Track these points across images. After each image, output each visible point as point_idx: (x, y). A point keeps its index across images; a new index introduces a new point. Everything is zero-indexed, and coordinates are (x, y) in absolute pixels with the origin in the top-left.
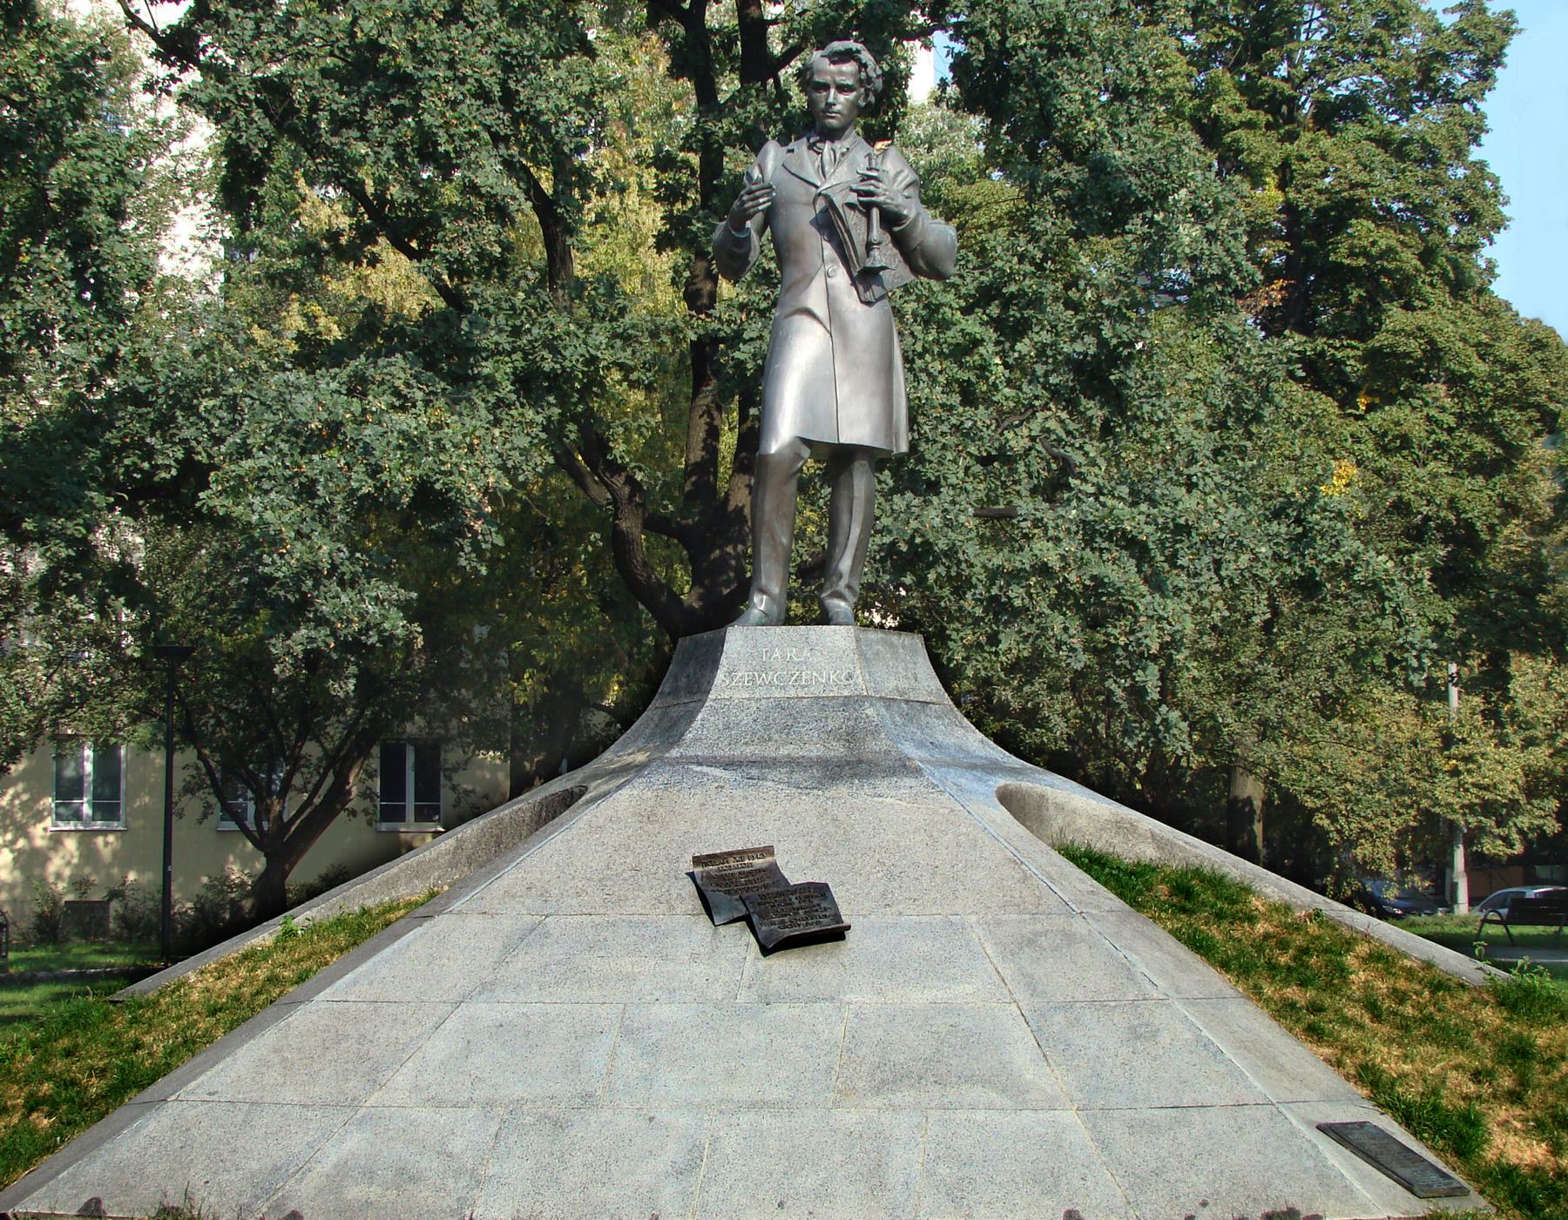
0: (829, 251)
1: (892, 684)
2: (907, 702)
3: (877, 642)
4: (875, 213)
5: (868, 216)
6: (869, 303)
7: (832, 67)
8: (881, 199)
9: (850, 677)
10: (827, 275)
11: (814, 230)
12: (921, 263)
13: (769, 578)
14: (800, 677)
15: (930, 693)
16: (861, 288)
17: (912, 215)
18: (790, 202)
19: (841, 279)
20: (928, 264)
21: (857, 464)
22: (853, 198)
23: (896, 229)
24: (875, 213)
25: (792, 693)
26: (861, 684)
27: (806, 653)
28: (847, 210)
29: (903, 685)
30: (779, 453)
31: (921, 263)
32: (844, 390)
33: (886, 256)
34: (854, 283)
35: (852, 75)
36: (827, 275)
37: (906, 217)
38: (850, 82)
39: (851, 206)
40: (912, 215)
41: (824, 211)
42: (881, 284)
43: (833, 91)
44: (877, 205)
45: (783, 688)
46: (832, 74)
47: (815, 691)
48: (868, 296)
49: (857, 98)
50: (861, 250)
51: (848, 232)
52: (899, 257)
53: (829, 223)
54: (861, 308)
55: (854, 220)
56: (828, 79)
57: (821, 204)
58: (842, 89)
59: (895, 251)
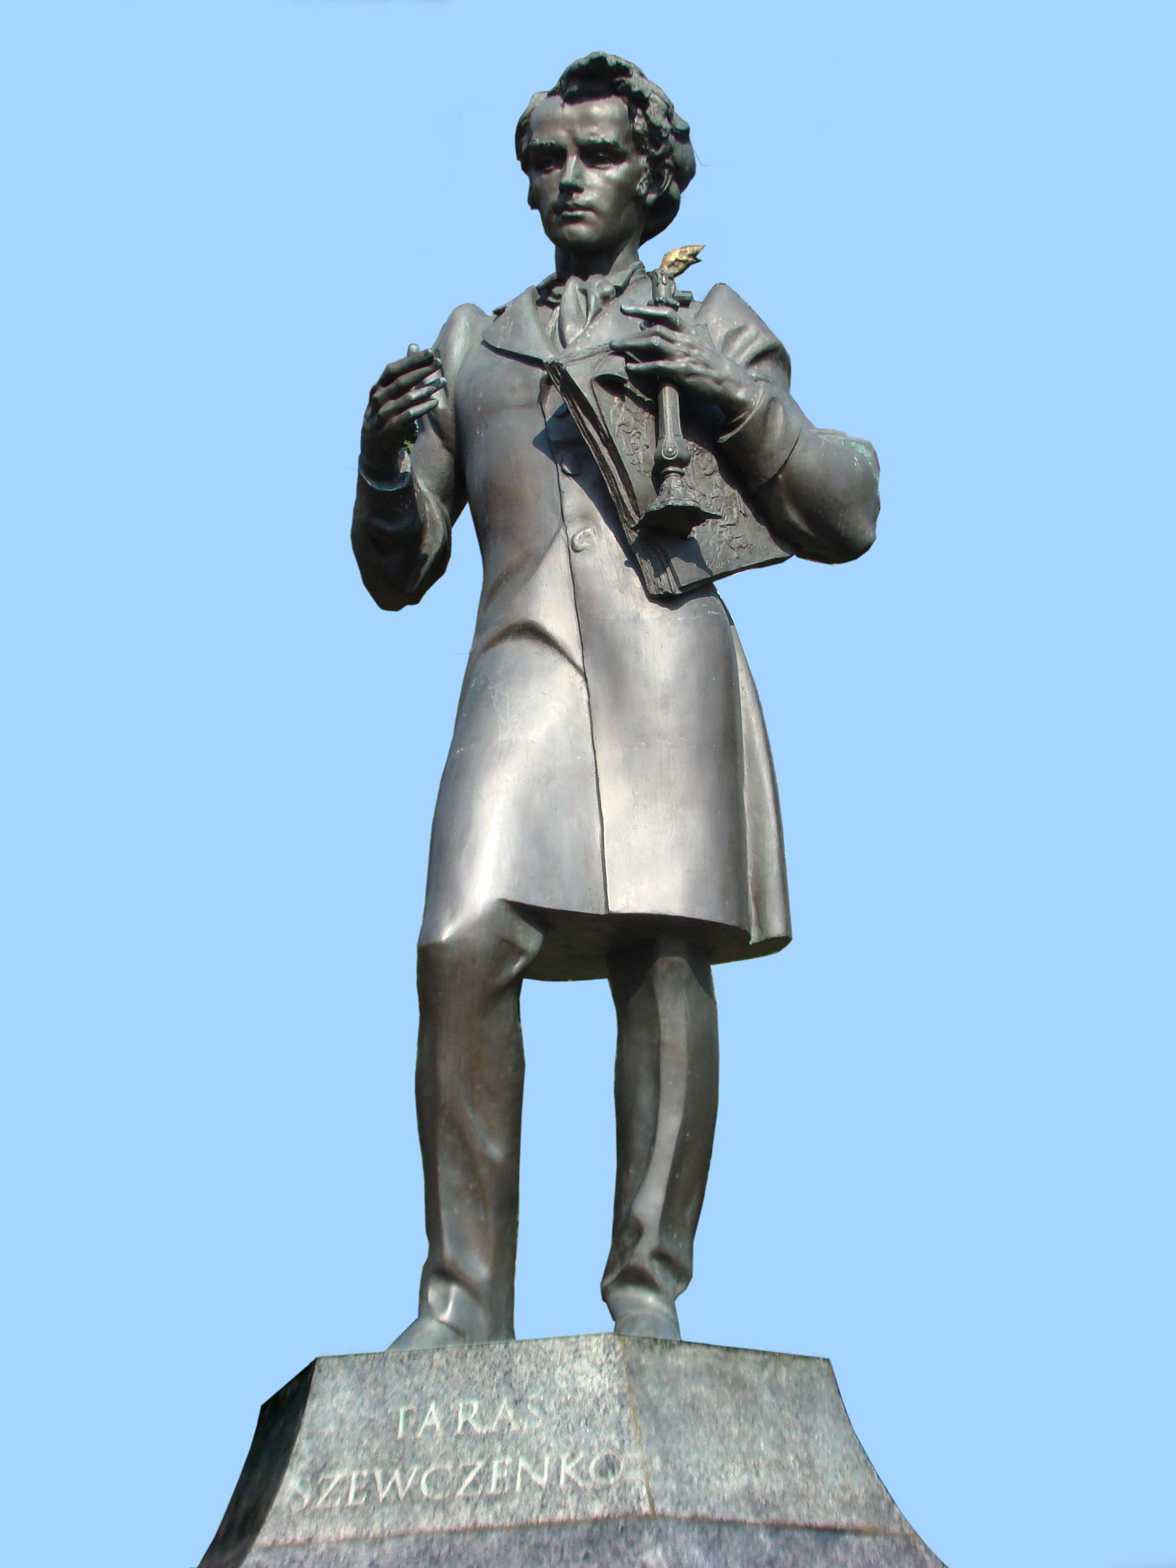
0: (576, 497)
1: (735, 1481)
2: (776, 1528)
3: (695, 1375)
4: (669, 398)
5: (654, 408)
6: (667, 600)
7: (569, 110)
8: (680, 364)
9: (609, 1466)
10: (573, 548)
11: (541, 458)
12: (794, 516)
13: (460, 1242)
14: (484, 1476)
15: (849, 1506)
16: (647, 566)
17: (758, 401)
18: (492, 408)
19: (603, 548)
20: (808, 515)
21: (662, 965)
22: (617, 366)
23: (725, 438)
24: (669, 398)
25: (463, 1517)
26: (640, 1480)
27: (505, 1410)
28: (604, 395)
29: (768, 1483)
30: (459, 941)
31: (794, 516)
32: (616, 797)
33: (699, 484)
34: (632, 562)
35: (613, 122)
36: (573, 548)
37: (742, 406)
38: (608, 135)
39: (610, 383)
40: (758, 401)
41: (562, 415)
42: (693, 554)
43: (573, 161)
44: (672, 378)
45: (443, 1505)
46: (568, 123)
47: (522, 1508)
48: (666, 582)
49: (634, 176)
50: (641, 480)
51: (608, 442)
52: (740, 505)
53: (573, 444)
54: (652, 613)
55: (617, 413)
56: (561, 136)
57: (554, 400)
58: (595, 154)
59: (728, 490)
